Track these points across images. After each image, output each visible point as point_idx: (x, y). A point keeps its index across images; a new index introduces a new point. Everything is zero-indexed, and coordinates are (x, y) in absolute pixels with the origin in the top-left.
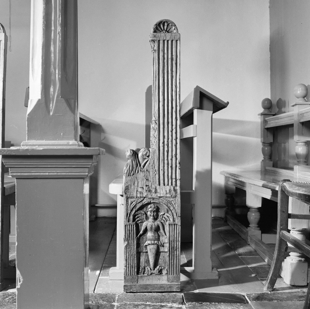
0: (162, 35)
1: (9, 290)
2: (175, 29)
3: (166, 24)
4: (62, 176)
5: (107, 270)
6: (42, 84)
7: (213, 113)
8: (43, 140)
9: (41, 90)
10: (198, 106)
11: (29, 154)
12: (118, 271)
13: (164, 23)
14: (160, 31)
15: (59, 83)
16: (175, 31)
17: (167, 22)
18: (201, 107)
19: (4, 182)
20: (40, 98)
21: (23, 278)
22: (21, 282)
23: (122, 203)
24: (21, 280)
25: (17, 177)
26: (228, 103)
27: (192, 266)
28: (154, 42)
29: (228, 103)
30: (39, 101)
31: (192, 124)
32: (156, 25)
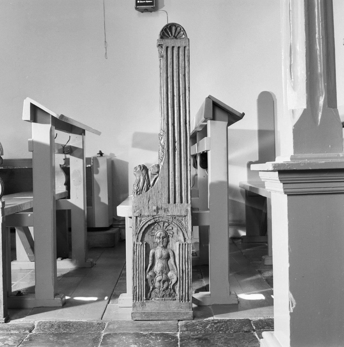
0: (169, 42)
1: (209, 318)
2: (183, 34)
3: (174, 28)
4: (329, 191)
5: (116, 300)
6: (307, 92)
7: (229, 124)
8: (311, 153)
9: (306, 100)
10: (211, 117)
11: (310, 168)
12: (126, 299)
13: (170, 27)
14: (166, 36)
15: (325, 91)
16: (184, 36)
17: (175, 26)
18: (214, 119)
19: (5, 204)
20: (305, 107)
21: (296, 301)
22: (294, 306)
23: (131, 226)
24: (294, 305)
25: (289, 194)
26: (244, 114)
27: (209, 291)
28: (162, 47)
29: (244, 114)
30: (305, 110)
31: (206, 136)
32: (162, 30)
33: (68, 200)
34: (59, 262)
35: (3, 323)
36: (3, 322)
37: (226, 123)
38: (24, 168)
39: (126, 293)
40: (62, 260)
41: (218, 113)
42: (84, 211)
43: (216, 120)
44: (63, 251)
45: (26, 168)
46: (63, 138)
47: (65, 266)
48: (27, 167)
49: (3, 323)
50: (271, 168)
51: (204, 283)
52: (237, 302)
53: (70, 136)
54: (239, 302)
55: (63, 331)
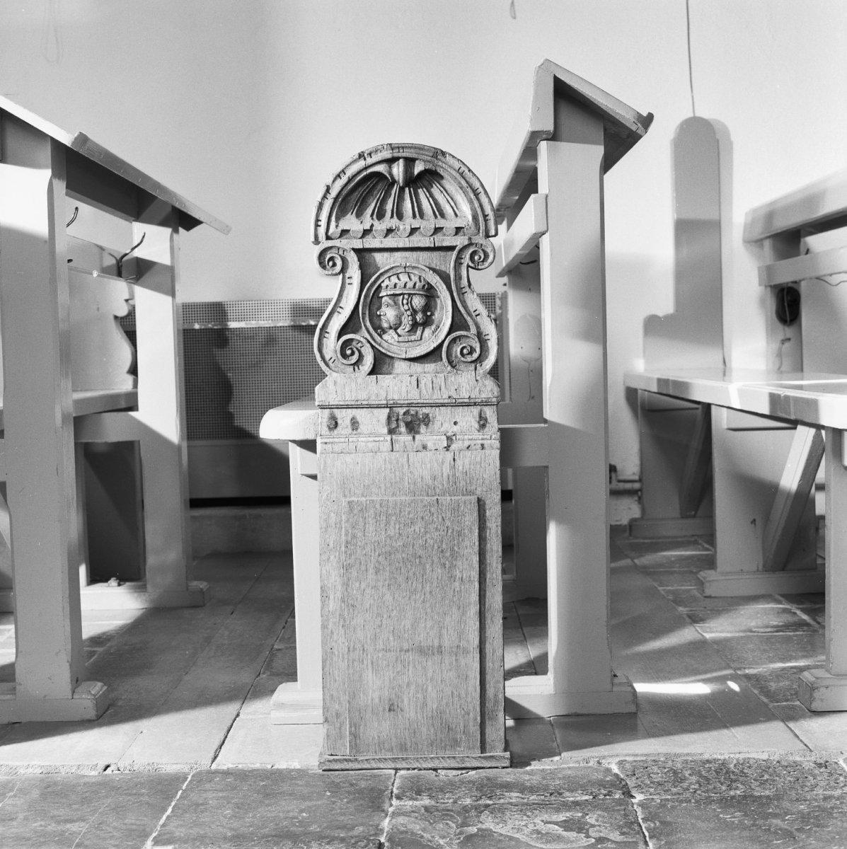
31: (536, 191)
33: (132, 414)
34: (85, 592)
35: (504, 768)
36: (505, 765)
37: (598, 151)
38: (304, 324)
39: (296, 681)
40: (119, 585)
41: (573, 120)
42: (179, 448)
43: (557, 141)
44: (110, 558)
45: (311, 326)
46: (99, 227)
47: (110, 606)
48: (197, 326)
49: (504, 768)
50: (382, 285)
51: (533, 652)
52: (632, 709)
53: (68, 225)
54: (637, 705)
55: (729, 789)
